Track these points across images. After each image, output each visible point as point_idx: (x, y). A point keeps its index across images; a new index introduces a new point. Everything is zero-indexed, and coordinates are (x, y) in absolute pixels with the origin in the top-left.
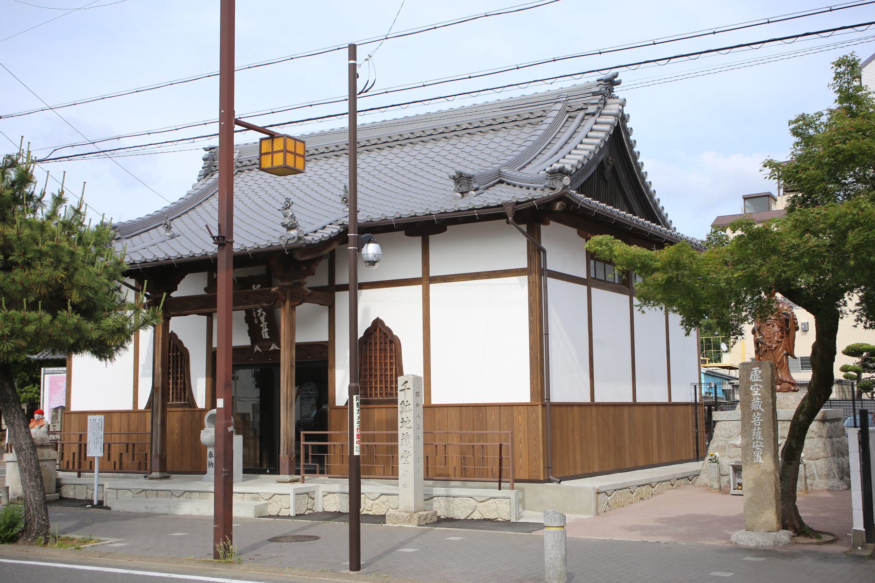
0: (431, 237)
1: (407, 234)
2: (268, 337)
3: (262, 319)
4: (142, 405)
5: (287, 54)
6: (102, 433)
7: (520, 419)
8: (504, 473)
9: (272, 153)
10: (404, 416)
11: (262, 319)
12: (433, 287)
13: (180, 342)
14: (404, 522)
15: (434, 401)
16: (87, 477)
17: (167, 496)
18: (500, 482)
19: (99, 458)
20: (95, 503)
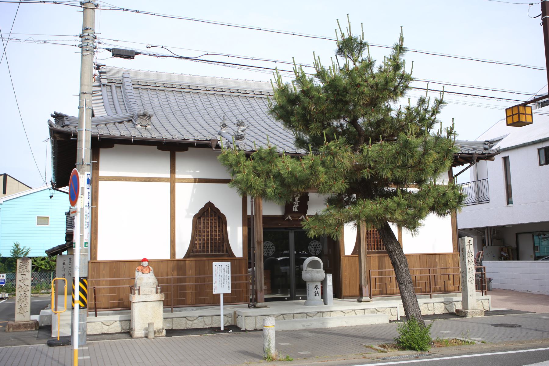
0: (177, 153)
1: (158, 148)
2: (296, 210)
3: (297, 199)
4: (181, 254)
5: (443, 53)
6: (230, 275)
7: (450, 261)
8: (392, 292)
9: (513, 115)
10: (470, 259)
11: (297, 199)
12: (168, 184)
13: (218, 210)
14: (479, 315)
15: (101, 257)
16: (176, 311)
17: (303, 317)
18: (96, 311)
19: (225, 295)
20: (222, 329)
